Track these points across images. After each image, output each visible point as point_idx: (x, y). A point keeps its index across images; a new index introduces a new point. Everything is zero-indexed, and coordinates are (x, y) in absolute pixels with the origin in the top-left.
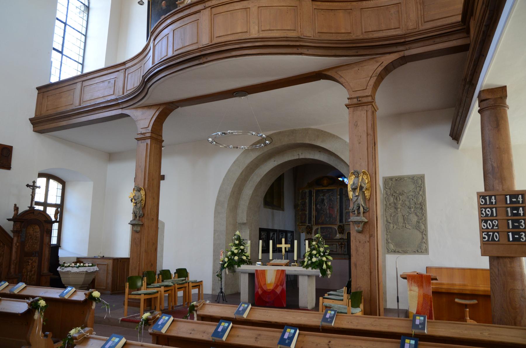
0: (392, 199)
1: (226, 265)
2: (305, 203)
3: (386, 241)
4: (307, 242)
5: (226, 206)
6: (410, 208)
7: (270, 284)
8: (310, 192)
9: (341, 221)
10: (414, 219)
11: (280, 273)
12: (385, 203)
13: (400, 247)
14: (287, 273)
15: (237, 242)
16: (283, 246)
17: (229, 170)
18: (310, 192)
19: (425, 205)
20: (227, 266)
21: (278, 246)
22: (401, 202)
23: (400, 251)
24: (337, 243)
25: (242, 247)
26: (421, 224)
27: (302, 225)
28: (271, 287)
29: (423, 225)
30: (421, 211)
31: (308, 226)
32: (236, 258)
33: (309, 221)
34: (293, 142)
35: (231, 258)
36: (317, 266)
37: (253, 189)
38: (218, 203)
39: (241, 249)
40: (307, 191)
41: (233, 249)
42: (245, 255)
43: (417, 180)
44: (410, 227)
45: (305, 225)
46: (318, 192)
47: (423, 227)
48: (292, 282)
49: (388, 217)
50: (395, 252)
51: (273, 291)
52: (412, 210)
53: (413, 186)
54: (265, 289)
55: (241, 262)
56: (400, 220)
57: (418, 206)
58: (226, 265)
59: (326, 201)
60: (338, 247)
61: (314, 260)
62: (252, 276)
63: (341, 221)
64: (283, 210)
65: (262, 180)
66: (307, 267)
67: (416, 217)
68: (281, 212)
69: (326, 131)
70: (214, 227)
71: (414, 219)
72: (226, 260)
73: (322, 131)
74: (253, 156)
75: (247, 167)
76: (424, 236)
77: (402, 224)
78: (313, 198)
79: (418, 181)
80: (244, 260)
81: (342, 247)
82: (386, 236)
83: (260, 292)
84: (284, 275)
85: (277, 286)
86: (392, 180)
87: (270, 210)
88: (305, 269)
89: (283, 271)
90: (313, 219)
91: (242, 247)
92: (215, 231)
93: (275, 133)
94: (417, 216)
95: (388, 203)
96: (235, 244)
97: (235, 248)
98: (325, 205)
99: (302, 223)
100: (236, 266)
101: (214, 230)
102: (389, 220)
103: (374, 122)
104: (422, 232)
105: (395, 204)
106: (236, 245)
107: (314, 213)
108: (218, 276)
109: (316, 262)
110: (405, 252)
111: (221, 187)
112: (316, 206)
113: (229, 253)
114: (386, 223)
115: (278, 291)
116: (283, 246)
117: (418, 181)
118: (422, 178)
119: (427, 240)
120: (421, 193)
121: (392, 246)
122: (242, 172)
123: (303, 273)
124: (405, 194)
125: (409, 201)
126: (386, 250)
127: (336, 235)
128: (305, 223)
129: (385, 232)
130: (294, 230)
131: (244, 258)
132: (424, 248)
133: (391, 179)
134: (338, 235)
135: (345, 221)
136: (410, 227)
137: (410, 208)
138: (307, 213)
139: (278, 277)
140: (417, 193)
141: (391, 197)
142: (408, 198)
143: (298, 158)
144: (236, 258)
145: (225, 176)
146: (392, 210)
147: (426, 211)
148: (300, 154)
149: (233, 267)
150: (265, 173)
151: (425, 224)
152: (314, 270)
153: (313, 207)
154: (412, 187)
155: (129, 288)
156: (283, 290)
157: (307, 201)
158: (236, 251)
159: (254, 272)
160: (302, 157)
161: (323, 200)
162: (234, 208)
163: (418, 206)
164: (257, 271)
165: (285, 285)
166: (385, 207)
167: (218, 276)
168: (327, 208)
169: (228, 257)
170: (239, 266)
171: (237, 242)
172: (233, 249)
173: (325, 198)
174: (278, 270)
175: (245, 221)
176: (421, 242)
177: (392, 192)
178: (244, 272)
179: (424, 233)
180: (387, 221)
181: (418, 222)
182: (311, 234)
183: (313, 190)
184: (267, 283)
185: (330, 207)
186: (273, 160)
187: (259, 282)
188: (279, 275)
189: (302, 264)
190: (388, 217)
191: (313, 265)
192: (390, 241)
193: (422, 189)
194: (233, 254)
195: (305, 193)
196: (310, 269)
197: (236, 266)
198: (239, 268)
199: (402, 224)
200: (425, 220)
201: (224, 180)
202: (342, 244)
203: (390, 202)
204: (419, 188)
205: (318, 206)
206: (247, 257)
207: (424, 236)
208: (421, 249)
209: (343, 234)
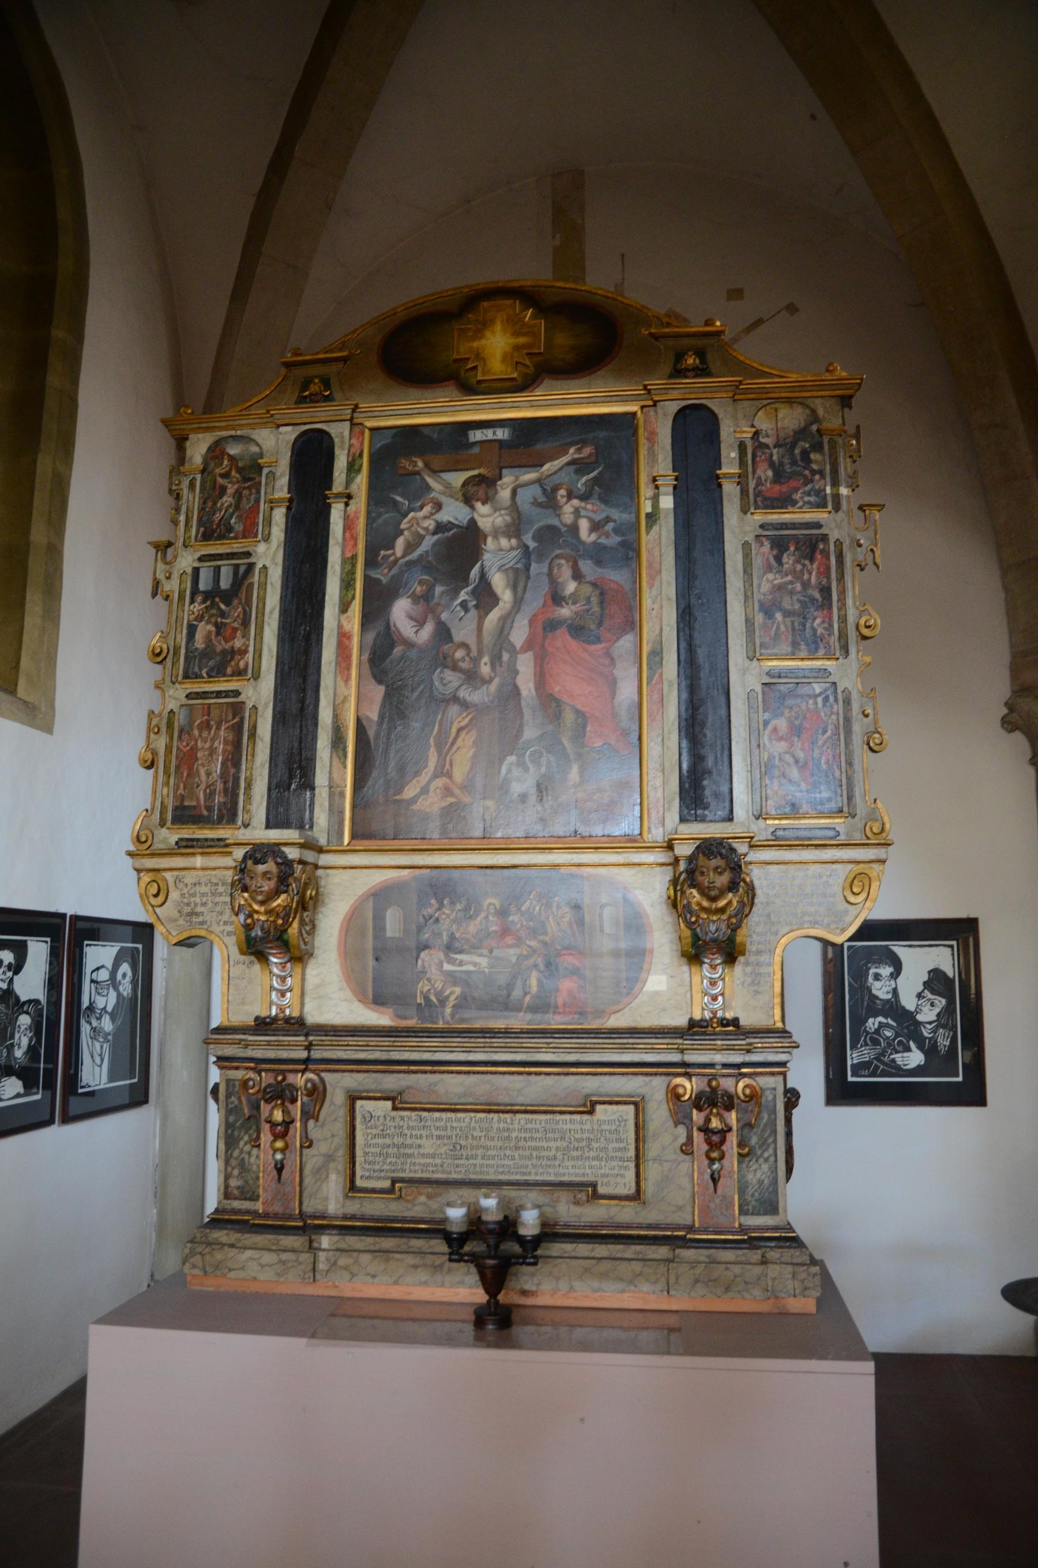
2: (243, 577)
8: (313, 457)
18: (313, 457)
21: (51, 1066)
24: (654, 1088)
27: (186, 846)
31: (259, 853)
33: (278, 789)
40: (275, 443)
45: (221, 846)
46: (400, 456)
60: (666, 1135)
78: (344, 525)
81: (715, 1140)
90: (332, 772)
98: (486, 598)
99: (183, 815)
103: (697, 758)
112: (376, 603)
128: (229, 815)
138: (261, 693)
153: (340, 620)
155: (131, 1084)
157: (270, 555)
161: (461, 548)
182: (299, 957)
183: (340, 432)
195: (251, 471)
202: (711, 1099)
205: (401, 611)
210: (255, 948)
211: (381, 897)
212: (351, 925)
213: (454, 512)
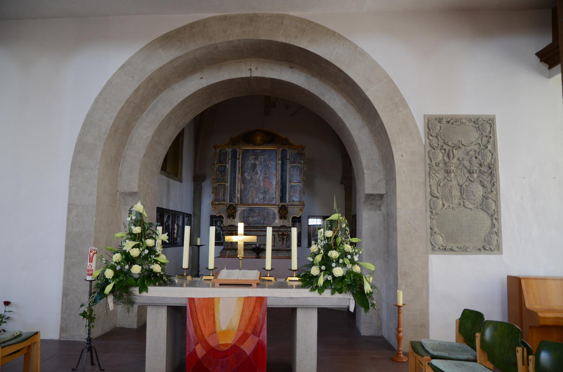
0: (441, 155)
1: (109, 288)
3: (429, 230)
4: (213, 229)
5: (99, 154)
6: (471, 172)
7: (227, 332)
8: (234, 153)
9: (283, 198)
10: (479, 191)
11: (253, 303)
12: (428, 161)
13: (452, 240)
14: (271, 303)
15: (137, 230)
16: (240, 238)
17: (109, 83)
18: (234, 153)
19: (496, 169)
20: (112, 292)
22: (455, 161)
23: (455, 248)
25: (150, 242)
26: (490, 201)
28: (230, 340)
29: (493, 204)
30: (489, 179)
32: (136, 269)
34: (252, 37)
35: (121, 270)
36: (349, 286)
37: (156, 126)
38: (81, 147)
39: (147, 248)
40: (229, 150)
41: (128, 246)
42: (156, 262)
43: (482, 125)
44: (470, 206)
45: (224, 204)
47: (493, 206)
48: (282, 320)
49: (434, 187)
50: (445, 249)
51: (235, 349)
52: (475, 175)
53: (477, 135)
54: (213, 344)
55: (150, 278)
56: (456, 193)
57: (484, 169)
58: (109, 288)
59: (258, 169)
61: (338, 272)
62: (177, 313)
63: (283, 198)
64: (181, 181)
65: (173, 112)
66: (321, 290)
67: (481, 188)
68: (179, 183)
69: (319, 22)
70: (70, 197)
71: (479, 191)
72: (109, 274)
73: (310, 22)
74: (166, 57)
75: (150, 79)
76: (494, 221)
77: (457, 201)
79: (485, 127)
80: (156, 273)
81: (283, 239)
82: (429, 221)
83: (200, 352)
84: (264, 309)
85: (244, 337)
86: (440, 122)
87: (165, 178)
88: (316, 294)
89: (261, 300)
91: (150, 242)
92: (71, 207)
93: (214, 18)
94: (483, 186)
95: (434, 162)
96: (131, 233)
97: (133, 243)
98: (257, 173)
100: (136, 290)
101: (69, 205)
102: (435, 192)
104: (492, 216)
105: (445, 163)
106: (133, 237)
107: (238, 186)
108: (84, 315)
109: (343, 277)
110: (464, 250)
111: (88, 116)
113: (117, 257)
114: (429, 197)
115: (248, 347)
116: (240, 238)
117: (485, 127)
118: (491, 121)
119: (499, 229)
120: (490, 147)
121: (440, 240)
122: (138, 89)
123: (310, 303)
124: (463, 147)
125: (470, 161)
126: (430, 247)
127: (274, 221)
129: (429, 214)
130: (192, 213)
131: (157, 268)
132: (495, 243)
133: (440, 119)
134: (277, 221)
135: (289, 199)
136: (470, 206)
137: (471, 172)
138: (228, 184)
139: (248, 314)
140: (482, 147)
141: (438, 151)
142: (468, 154)
143: (248, 75)
144: (136, 269)
145: (100, 94)
146: (441, 175)
147: (497, 178)
148: (253, 70)
149: (130, 294)
150: (181, 99)
151: (497, 202)
152: (337, 295)
154: (474, 136)
156: (259, 346)
157: (228, 166)
158: (135, 253)
159: (184, 303)
160: (257, 74)
162: (114, 161)
163: (484, 169)
164: (191, 300)
165: (264, 333)
166: (428, 169)
167: (84, 315)
168: (261, 178)
169: (113, 268)
170: (143, 288)
171: (137, 230)
172: (128, 246)
173: (257, 163)
174: (247, 299)
175: (136, 190)
176: (491, 233)
177: (441, 142)
178: (157, 305)
179: (495, 216)
180: (432, 195)
181: (485, 197)
182: (234, 217)
183: (238, 150)
184: (218, 330)
185: (265, 178)
186: (197, 76)
187: (197, 328)
188: (251, 308)
189: (308, 281)
190: (434, 187)
191: (337, 285)
192: (436, 229)
193: (491, 140)
194: (129, 259)
196: (327, 293)
197: (136, 290)
198: (144, 294)
199: (457, 201)
200: (497, 194)
201: (97, 101)
203: (438, 161)
204: (487, 139)
205: (246, 174)
206: (162, 264)
207: (494, 221)
208: (489, 244)
209: (285, 218)
210: (229, 217)
211: (244, 211)
212: (240, 214)
213: (252, 162)
